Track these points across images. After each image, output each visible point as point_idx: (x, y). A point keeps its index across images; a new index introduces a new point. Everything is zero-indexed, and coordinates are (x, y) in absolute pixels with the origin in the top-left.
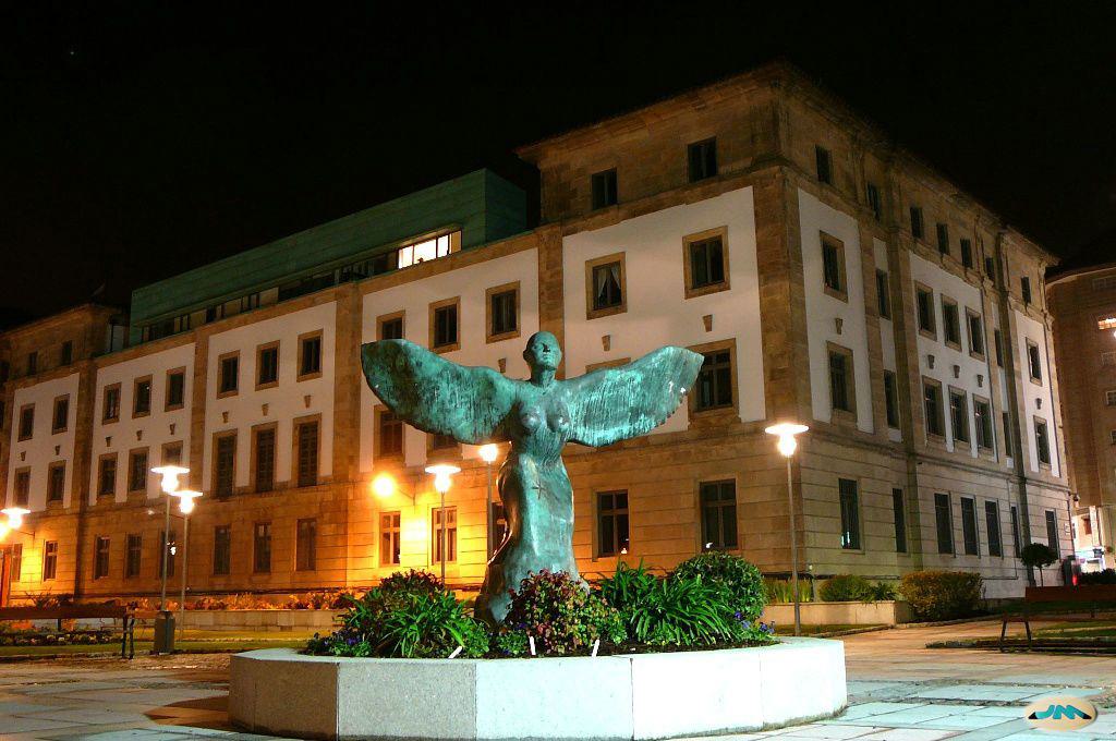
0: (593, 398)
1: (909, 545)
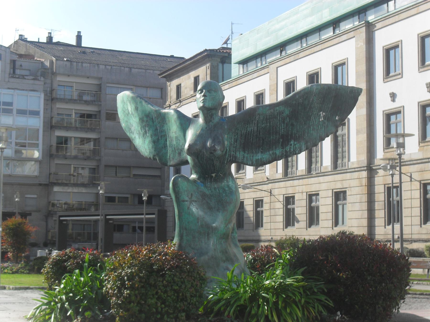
0: (249, 129)
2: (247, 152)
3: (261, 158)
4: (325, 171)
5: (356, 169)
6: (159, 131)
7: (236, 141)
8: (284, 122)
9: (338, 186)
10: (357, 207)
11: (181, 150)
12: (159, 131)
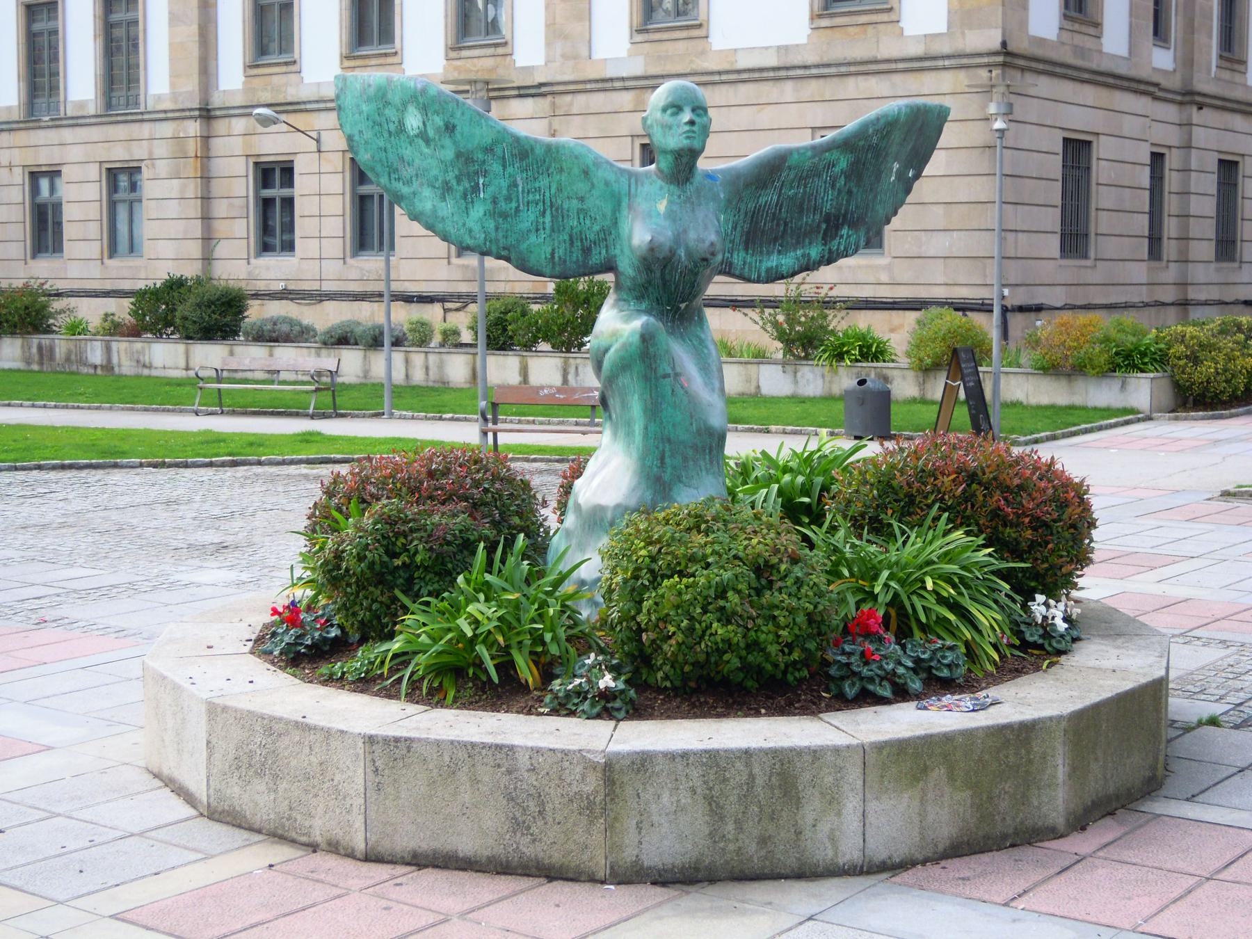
0: (762, 200)
1: (1170, 248)
2: (750, 251)
3: (777, 266)
4: (80, 114)
5: (170, 115)
6: (520, 189)
7: (734, 228)
8: (833, 186)
9: (119, 155)
10: (173, 209)
11: (595, 243)
12: (523, 191)
